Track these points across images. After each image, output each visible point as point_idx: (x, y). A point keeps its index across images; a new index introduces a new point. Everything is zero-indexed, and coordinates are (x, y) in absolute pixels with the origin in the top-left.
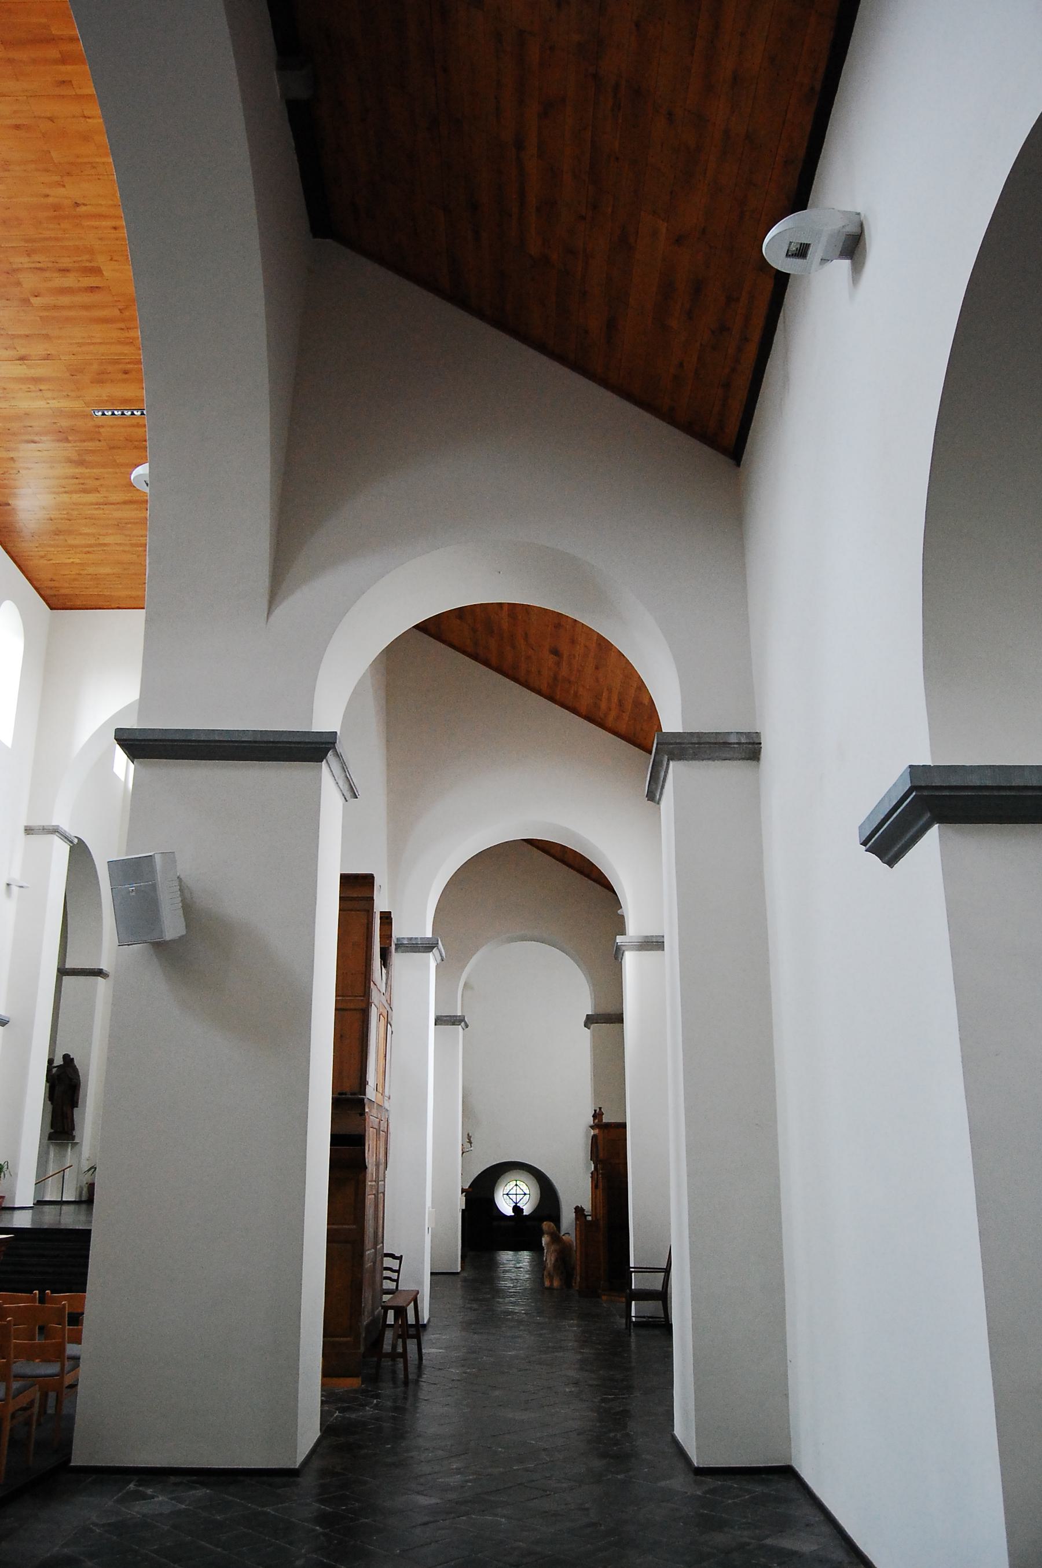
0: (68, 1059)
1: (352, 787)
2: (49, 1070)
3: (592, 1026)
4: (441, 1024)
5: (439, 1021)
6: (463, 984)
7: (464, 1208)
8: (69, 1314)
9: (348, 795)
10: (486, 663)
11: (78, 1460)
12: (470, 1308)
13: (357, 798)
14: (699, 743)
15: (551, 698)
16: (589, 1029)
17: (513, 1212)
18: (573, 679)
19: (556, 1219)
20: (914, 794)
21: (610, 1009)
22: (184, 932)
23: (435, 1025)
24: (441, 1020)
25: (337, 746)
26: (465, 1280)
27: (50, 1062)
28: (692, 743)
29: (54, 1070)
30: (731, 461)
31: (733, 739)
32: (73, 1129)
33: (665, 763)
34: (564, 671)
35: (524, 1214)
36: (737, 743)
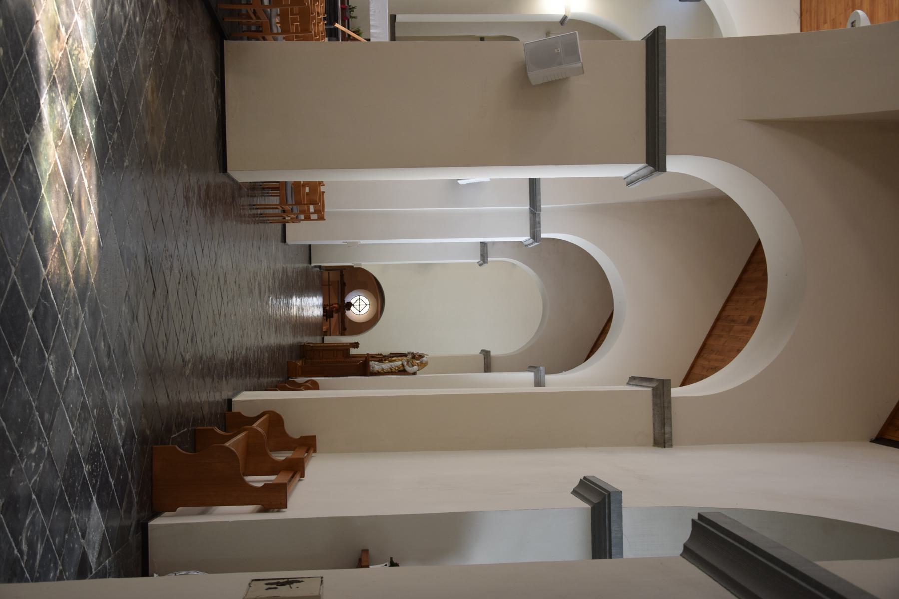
1: (633, 182)
3: (482, 356)
4: (481, 246)
5: (484, 245)
6: (515, 263)
7: (354, 267)
9: (629, 180)
10: (744, 271)
11: (226, 43)
12: (293, 272)
13: (627, 185)
14: (664, 407)
15: (718, 319)
16: (480, 353)
17: (347, 303)
18: (731, 334)
19: (343, 332)
20: (606, 493)
21: (494, 364)
22: (533, 84)
23: (481, 242)
24: (484, 246)
25: (658, 173)
26: (307, 269)
28: (664, 403)
30: (875, 436)
31: (667, 429)
33: (651, 386)
34: (737, 328)
35: (346, 311)
36: (664, 432)
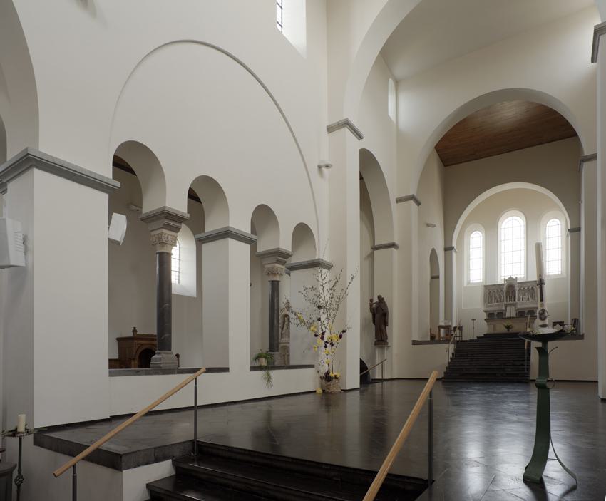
0: (381, 299)
2: (371, 306)
8: (390, 477)
21: (447, 252)
27: (371, 301)
29: (374, 306)
32: (387, 339)
